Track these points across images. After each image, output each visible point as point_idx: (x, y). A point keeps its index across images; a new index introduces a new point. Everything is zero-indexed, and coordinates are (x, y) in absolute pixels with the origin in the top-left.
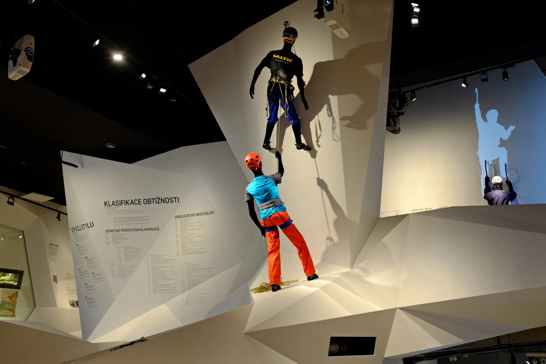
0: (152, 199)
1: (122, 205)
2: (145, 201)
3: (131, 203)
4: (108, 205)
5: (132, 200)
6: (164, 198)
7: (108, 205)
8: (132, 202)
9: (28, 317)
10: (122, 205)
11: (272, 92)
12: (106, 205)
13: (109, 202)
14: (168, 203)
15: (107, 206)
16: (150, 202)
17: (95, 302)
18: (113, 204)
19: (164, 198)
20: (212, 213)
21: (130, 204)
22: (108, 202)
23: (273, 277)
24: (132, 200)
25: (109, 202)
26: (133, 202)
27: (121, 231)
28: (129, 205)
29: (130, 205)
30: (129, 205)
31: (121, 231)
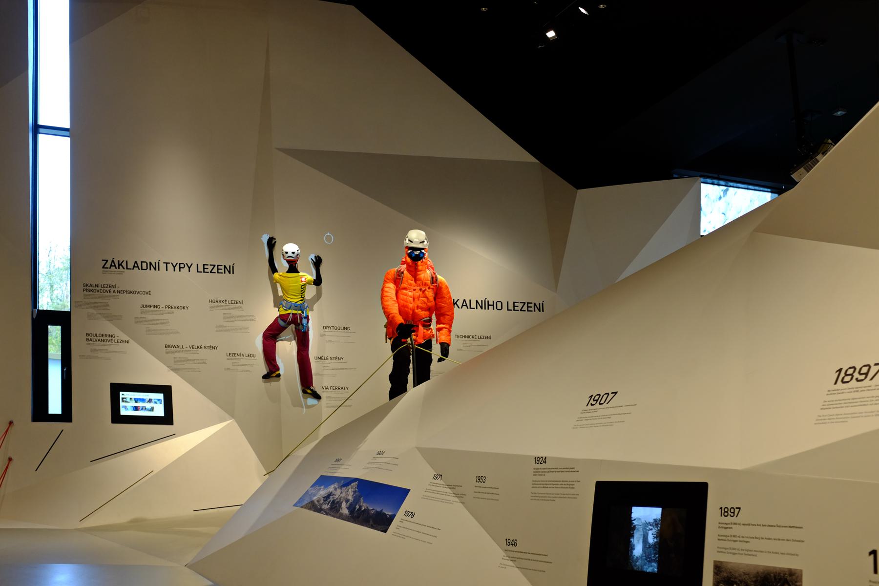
0: (737, 508)
1: (488, 309)
2: (499, 307)
3: (463, 305)
4: (125, 267)
5: (464, 300)
6: (150, 269)
7: (125, 267)
8: (465, 304)
9: (383, 364)
10: (488, 309)
11: (410, 354)
12: (121, 267)
13: (127, 262)
14: (498, 302)
15: (124, 268)
16: (726, 514)
17: (780, 573)
18: (134, 267)
19: (150, 269)
20: (540, 308)
21: (460, 307)
22: (125, 262)
23: (444, 287)
24: (464, 300)
25: (127, 262)
26: (114, 263)
27: (329, 388)
28: (459, 308)
29: (460, 309)
30: (459, 308)
31: (329, 388)
